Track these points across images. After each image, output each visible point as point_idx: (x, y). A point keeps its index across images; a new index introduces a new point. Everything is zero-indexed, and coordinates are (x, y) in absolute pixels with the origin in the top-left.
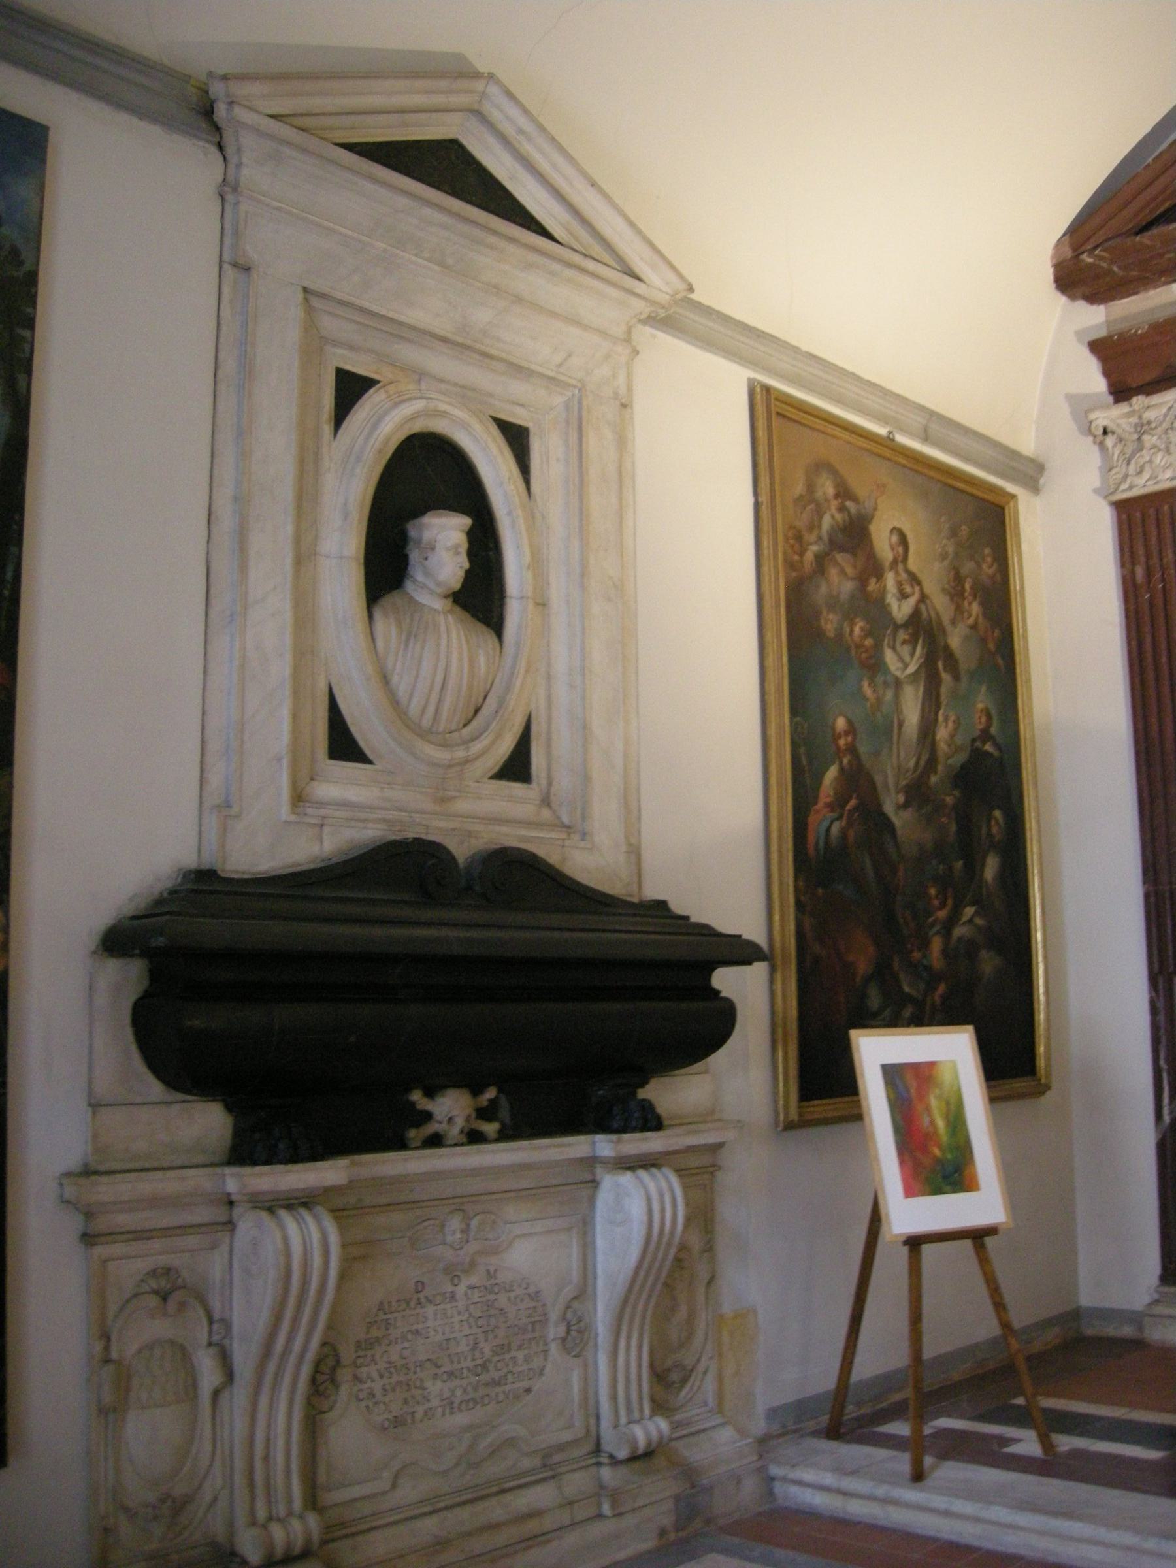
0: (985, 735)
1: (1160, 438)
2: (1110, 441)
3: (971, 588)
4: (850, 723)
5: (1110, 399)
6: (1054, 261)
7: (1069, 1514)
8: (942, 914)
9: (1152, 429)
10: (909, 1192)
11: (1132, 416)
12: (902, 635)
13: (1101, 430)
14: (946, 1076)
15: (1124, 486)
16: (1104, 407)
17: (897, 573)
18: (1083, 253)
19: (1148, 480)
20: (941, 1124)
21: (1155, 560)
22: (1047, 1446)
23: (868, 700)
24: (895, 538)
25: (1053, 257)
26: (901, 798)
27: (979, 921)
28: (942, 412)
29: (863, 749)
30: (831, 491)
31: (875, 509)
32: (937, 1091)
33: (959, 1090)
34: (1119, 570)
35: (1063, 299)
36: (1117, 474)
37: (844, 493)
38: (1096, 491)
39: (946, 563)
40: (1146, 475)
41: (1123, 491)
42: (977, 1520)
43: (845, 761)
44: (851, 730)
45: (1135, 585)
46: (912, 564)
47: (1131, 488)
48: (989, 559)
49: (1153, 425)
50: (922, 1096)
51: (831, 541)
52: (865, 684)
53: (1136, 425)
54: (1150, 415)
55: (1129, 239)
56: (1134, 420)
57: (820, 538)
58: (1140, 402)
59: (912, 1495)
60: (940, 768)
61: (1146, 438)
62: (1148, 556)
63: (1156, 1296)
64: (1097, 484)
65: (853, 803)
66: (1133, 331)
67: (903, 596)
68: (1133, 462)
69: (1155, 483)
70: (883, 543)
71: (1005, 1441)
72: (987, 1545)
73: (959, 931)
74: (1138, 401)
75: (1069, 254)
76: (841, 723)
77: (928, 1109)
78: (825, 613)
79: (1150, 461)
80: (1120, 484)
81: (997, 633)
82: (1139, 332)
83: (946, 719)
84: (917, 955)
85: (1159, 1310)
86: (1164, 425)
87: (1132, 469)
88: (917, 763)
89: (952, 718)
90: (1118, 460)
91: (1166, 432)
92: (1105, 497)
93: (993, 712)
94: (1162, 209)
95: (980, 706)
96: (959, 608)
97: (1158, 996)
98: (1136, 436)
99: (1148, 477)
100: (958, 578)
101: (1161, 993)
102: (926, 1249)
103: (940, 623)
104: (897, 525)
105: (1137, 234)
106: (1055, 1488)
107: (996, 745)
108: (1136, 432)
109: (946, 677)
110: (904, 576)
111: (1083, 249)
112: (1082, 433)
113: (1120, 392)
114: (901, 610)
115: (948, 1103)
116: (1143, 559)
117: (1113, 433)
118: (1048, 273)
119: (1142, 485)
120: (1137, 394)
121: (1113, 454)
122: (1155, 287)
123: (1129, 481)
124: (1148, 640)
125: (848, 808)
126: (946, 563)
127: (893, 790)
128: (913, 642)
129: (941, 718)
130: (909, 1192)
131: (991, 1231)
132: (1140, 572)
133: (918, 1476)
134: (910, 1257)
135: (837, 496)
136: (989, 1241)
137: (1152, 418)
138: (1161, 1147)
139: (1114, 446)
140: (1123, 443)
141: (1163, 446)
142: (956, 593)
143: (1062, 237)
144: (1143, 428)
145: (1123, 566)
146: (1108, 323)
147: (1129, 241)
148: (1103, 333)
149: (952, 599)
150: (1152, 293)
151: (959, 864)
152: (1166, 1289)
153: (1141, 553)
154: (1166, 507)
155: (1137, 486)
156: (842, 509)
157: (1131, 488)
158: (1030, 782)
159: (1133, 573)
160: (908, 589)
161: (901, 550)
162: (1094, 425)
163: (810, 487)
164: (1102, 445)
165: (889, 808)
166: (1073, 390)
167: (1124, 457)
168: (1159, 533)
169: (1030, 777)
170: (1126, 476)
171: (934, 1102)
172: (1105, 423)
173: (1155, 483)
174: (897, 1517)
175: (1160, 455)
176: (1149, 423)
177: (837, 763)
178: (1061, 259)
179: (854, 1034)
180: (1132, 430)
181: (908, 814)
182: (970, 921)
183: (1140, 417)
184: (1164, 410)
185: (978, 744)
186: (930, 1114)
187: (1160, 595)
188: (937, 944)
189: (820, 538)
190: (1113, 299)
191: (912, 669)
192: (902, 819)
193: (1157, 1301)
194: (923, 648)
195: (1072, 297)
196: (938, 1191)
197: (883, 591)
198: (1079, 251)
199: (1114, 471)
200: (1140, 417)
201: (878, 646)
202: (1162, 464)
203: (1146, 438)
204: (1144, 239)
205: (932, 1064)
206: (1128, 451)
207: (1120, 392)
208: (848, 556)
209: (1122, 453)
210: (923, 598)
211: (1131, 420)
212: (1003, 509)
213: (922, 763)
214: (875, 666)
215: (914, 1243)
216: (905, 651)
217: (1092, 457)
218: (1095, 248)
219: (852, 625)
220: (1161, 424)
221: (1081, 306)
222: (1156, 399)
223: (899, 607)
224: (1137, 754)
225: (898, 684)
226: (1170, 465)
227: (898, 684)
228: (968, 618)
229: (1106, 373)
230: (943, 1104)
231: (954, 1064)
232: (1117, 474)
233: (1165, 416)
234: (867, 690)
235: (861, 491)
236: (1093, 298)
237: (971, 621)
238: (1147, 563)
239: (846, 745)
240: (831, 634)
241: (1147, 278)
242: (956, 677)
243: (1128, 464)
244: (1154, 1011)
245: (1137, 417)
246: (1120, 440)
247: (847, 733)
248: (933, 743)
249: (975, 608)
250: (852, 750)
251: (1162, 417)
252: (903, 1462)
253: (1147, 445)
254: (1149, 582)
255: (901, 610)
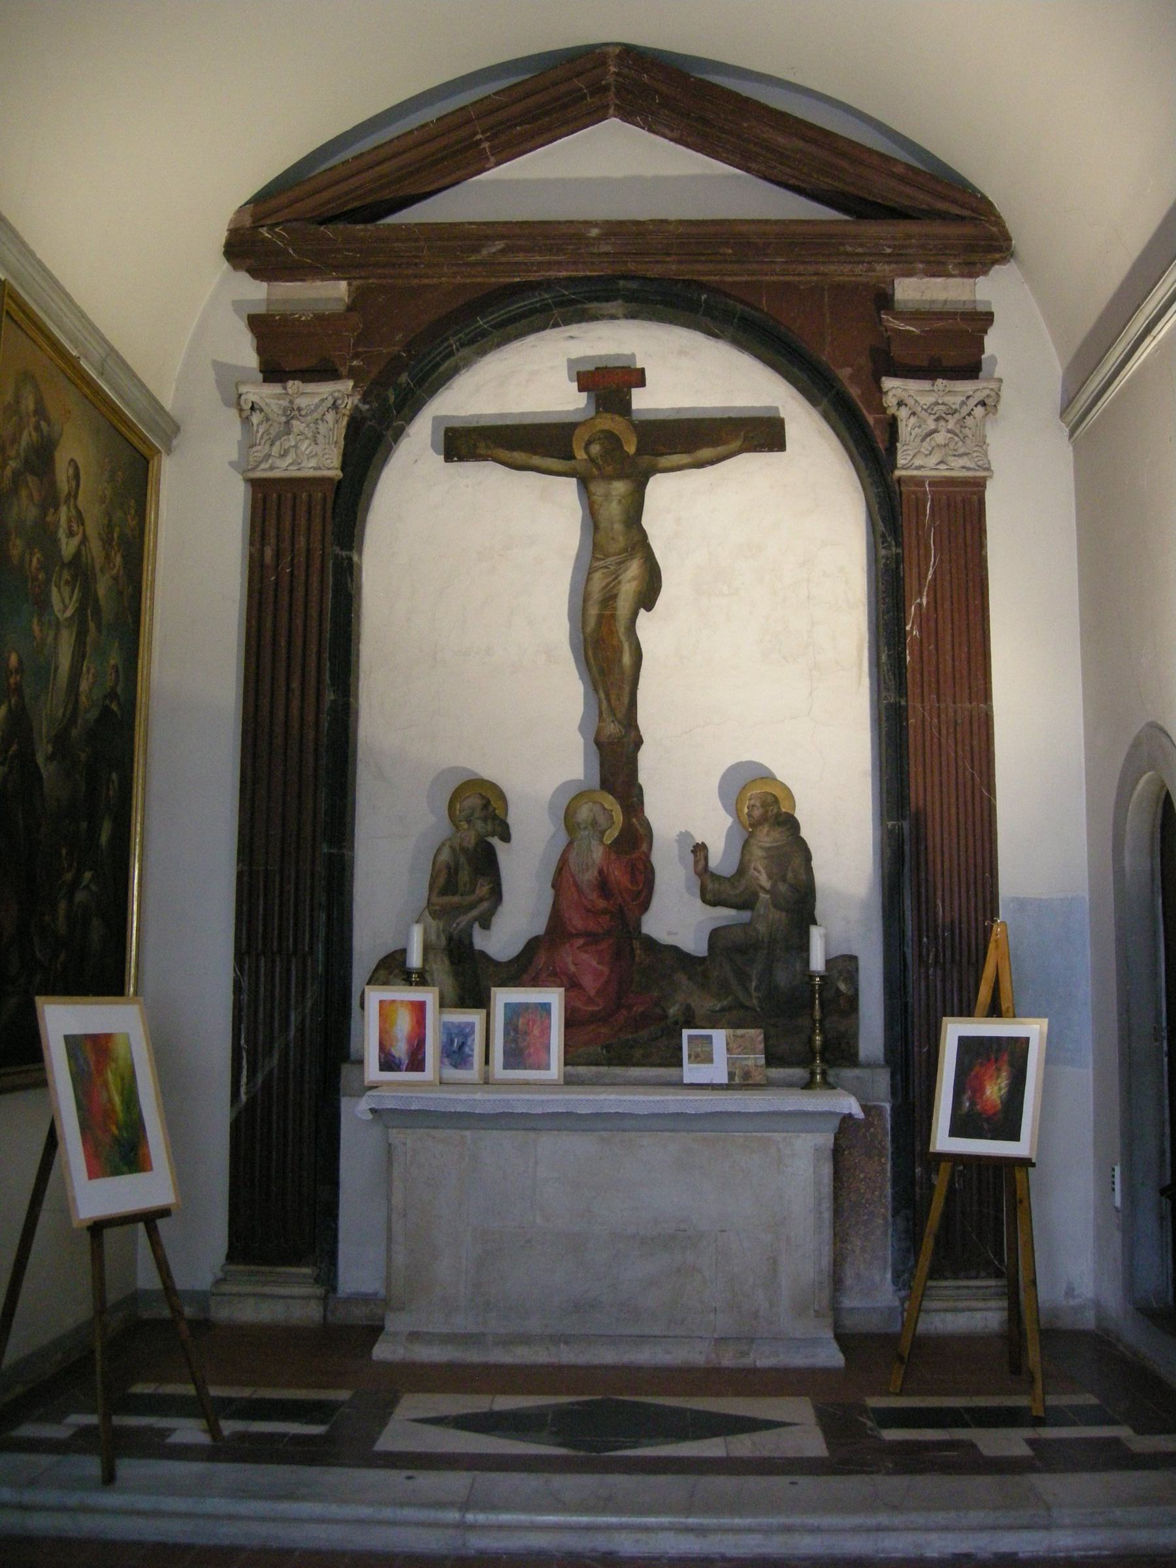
0: (112, 695)
1: (308, 426)
2: (256, 418)
3: (118, 538)
4: (20, 662)
5: (260, 376)
6: (232, 226)
7: (290, 1496)
8: (69, 876)
9: (300, 415)
10: (92, 1175)
11: (284, 399)
12: (66, 575)
13: (250, 405)
14: (119, 1049)
15: (263, 466)
16: (254, 383)
17: (69, 508)
18: (262, 226)
19: (290, 464)
20: (117, 1100)
21: (286, 545)
22: (214, 1431)
23: (35, 638)
24: (71, 471)
25: (231, 221)
26: (50, 749)
27: (94, 888)
28: (121, 353)
29: (28, 692)
30: (31, 407)
31: (61, 435)
32: (113, 1065)
33: (133, 1066)
34: (247, 546)
35: (226, 265)
36: (260, 451)
37: (40, 411)
38: (231, 464)
39: (104, 506)
40: (289, 460)
41: (263, 470)
42: (189, 1515)
43: (13, 701)
44: (20, 669)
45: (262, 565)
46: (82, 502)
47: (272, 468)
48: (133, 511)
49: (303, 413)
50: (101, 1072)
51: (26, 462)
52: (35, 621)
53: (285, 409)
54: (302, 402)
55: (313, 226)
56: (284, 403)
57: (18, 454)
58: (295, 387)
59: (110, 1499)
60: (80, 721)
61: (294, 422)
62: (278, 536)
63: (220, 1275)
64: (234, 456)
65: (14, 748)
66: (297, 316)
67: (71, 534)
68: (278, 443)
69: (299, 469)
70: (62, 473)
71: (165, 1433)
72: (201, 1541)
73: (80, 897)
74: (293, 385)
75: (247, 222)
76: (13, 659)
77: (106, 1084)
78: (13, 536)
79: (296, 447)
80: (260, 462)
81: (130, 589)
82: (303, 318)
83: (88, 670)
84: (47, 918)
85: (225, 1288)
86: (316, 415)
87: (275, 450)
88: (64, 715)
89: (92, 671)
90: (262, 437)
91: (316, 422)
92: (243, 472)
93: (120, 667)
94: (349, 207)
95: (112, 662)
96: (108, 557)
97: (242, 974)
98: (284, 419)
99: (291, 461)
100: (110, 527)
101: (246, 972)
102: (109, 1234)
103: (93, 567)
104: (75, 458)
105: (321, 224)
106: (227, 1472)
107: (119, 704)
108: (284, 414)
109: (92, 625)
110: (73, 512)
111: (261, 223)
112: (227, 403)
113: (272, 372)
114: (68, 547)
115: (123, 1079)
116: (273, 541)
117: (261, 410)
118: (222, 236)
119: (283, 468)
120: (294, 379)
121: (258, 431)
122: (323, 280)
123: (270, 461)
124: (269, 624)
125: (11, 752)
126: (104, 506)
127: (45, 741)
128: (71, 584)
129: (85, 669)
130: (92, 1175)
131: (164, 1212)
132: (269, 553)
133: (109, 1478)
134: (92, 1243)
135: (36, 412)
136: (161, 1223)
137: (303, 406)
138: (235, 1127)
139: (261, 423)
140: (269, 423)
141: (310, 435)
142: (107, 542)
143: (246, 204)
144: (292, 413)
145: (252, 544)
146: (269, 301)
147: (313, 227)
148: (261, 310)
149: (104, 547)
150: (319, 283)
151: (84, 825)
152: (233, 1268)
153: (272, 534)
154: (304, 495)
155: (278, 468)
156: (37, 428)
157: (272, 468)
158: (141, 749)
159: (262, 552)
160: (75, 528)
161: (74, 484)
162: (243, 398)
163: (18, 399)
164: (246, 421)
165: (40, 759)
166: (223, 358)
167: (267, 437)
168: (294, 519)
169: (142, 744)
170: (268, 456)
171: (110, 1076)
172: (255, 398)
173: (299, 469)
174: (87, 1525)
175: (307, 442)
176: (299, 409)
177: (7, 704)
178: (239, 225)
179: (39, 1000)
180: (280, 412)
181: (53, 766)
182: (87, 887)
183: (291, 402)
184: (317, 400)
185: (107, 702)
186: (108, 1090)
187: (287, 579)
188: (63, 906)
189: (18, 454)
190: (277, 279)
191: (68, 614)
192: (48, 770)
193: (224, 1280)
194: (79, 591)
195: (236, 267)
196: (116, 1172)
197: (57, 524)
198: (261, 223)
199: (255, 449)
200: (291, 402)
201: (48, 581)
202: (307, 452)
203: (294, 422)
204: (327, 231)
205: (108, 1037)
206: (273, 432)
207: (272, 372)
208: (35, 478)
209: (267, 432)
210: (84, 540)
211: (281, 402)
212: (147, 461)
213: (68, 712)
214: (42, 604)
215: (97, 1228)
216: (66, 591)
217: (235, 431)
218: (277, 224)
219: (32, 554)
220: (313, 411)
221: (243, 278)
222: (311, 387)
223: (67, 544)
224: (245, 733)
225: (58, 625)
226: (316, 454)
227: (58, 625)
228: (113, 569)
229: (260, 350)
230: (119, 1080)
231: (127, 1036)
232: (260, 451)
233: (317, 406)
234: (36, 628)
235: (54, 414)
236: (257, 273)
237: (115, 571)
238: (278, 545)
239: (16, 684)
240: (16, 561)
241: (317, 267)
242: (99, 629)
243: (271, 445)
244: (237, 989)
245: (288, 400)
246: (268, 420)
247: (17, 671)
248: (77, 695)
249: (118, 560)
250: (18, 690)
251: (312, 407)
252: (92, 1466)
253: (295, 430)
254: (277, 566)
255: (68, 547)
